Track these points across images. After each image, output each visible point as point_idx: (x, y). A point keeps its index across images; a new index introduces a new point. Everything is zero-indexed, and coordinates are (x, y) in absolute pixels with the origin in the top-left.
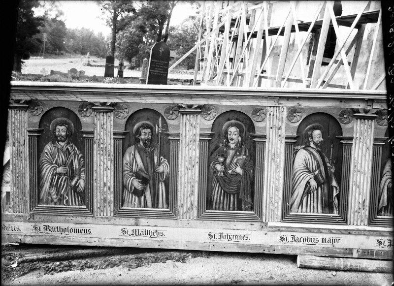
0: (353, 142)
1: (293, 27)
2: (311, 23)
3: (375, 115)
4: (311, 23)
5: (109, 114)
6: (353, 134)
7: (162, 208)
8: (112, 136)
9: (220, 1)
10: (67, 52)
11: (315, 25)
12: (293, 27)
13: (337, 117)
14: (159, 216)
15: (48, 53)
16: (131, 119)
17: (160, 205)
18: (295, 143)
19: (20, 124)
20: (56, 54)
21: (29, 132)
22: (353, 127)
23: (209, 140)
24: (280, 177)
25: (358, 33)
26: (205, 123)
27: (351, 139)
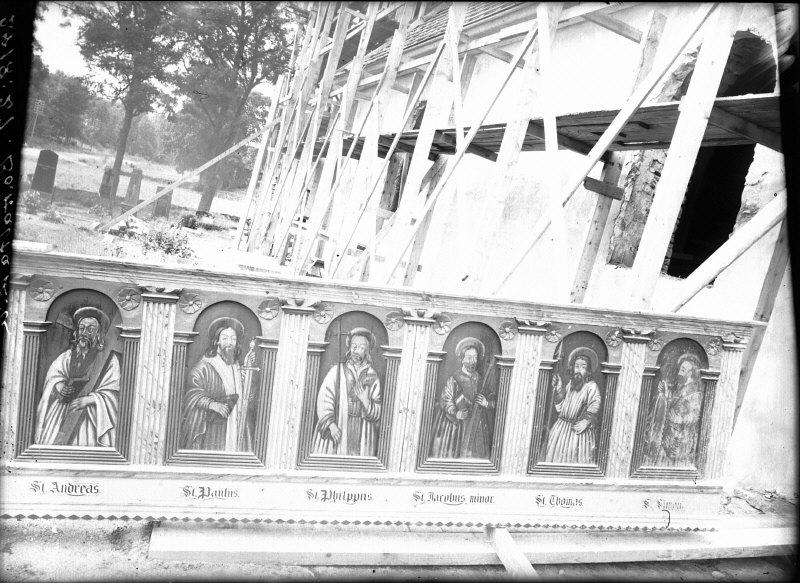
0: (515, 364)
1: (536, 126)
2: (394, 135)
3: (648, 339)
4: (615, 113)
5: (162, 305)
6: (140, 324)
7: (364, 453)
8: (22, 328)
9: (412, 3)
10: (84, 140)
11: (629, 122)
12: (536, 126)
13: (255, 310)
14: (364, 465)
15: (40, 136)
16: (455, 333)
17: (362, 452)
18: (322, 357)
19: (24, 311)
20: (60, 142)
21: (176, 335)
22: (141, 316)
23: (322, 352)
24: (631, 431)
25: (432, 169)
26: (314, 331)
27: (619, 368)
